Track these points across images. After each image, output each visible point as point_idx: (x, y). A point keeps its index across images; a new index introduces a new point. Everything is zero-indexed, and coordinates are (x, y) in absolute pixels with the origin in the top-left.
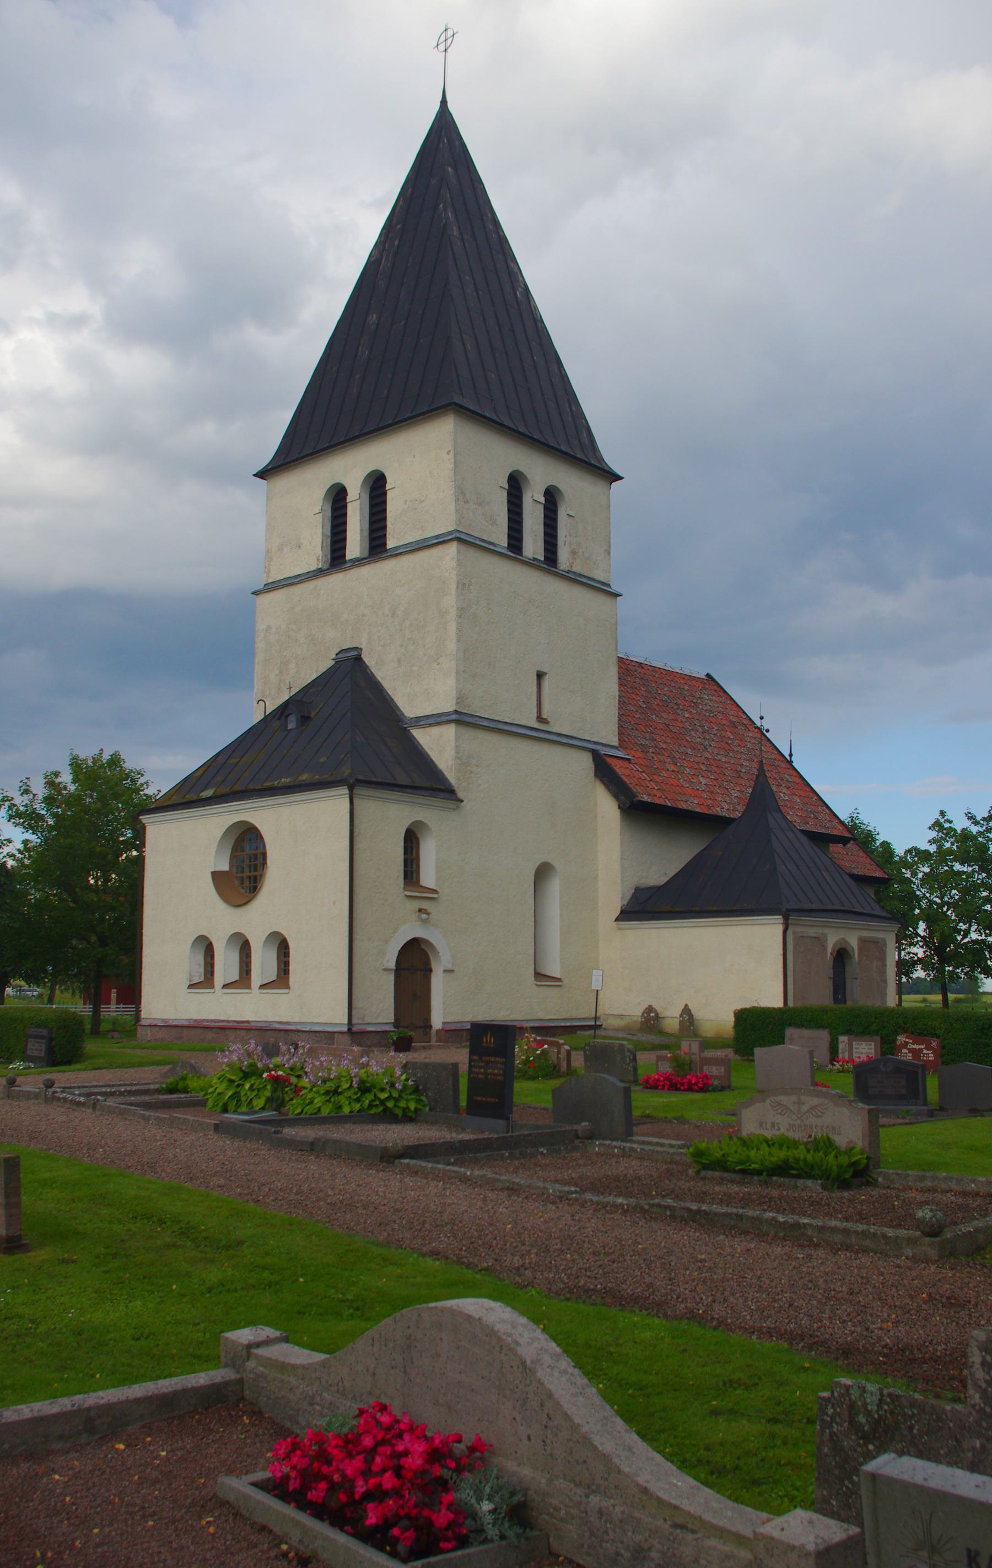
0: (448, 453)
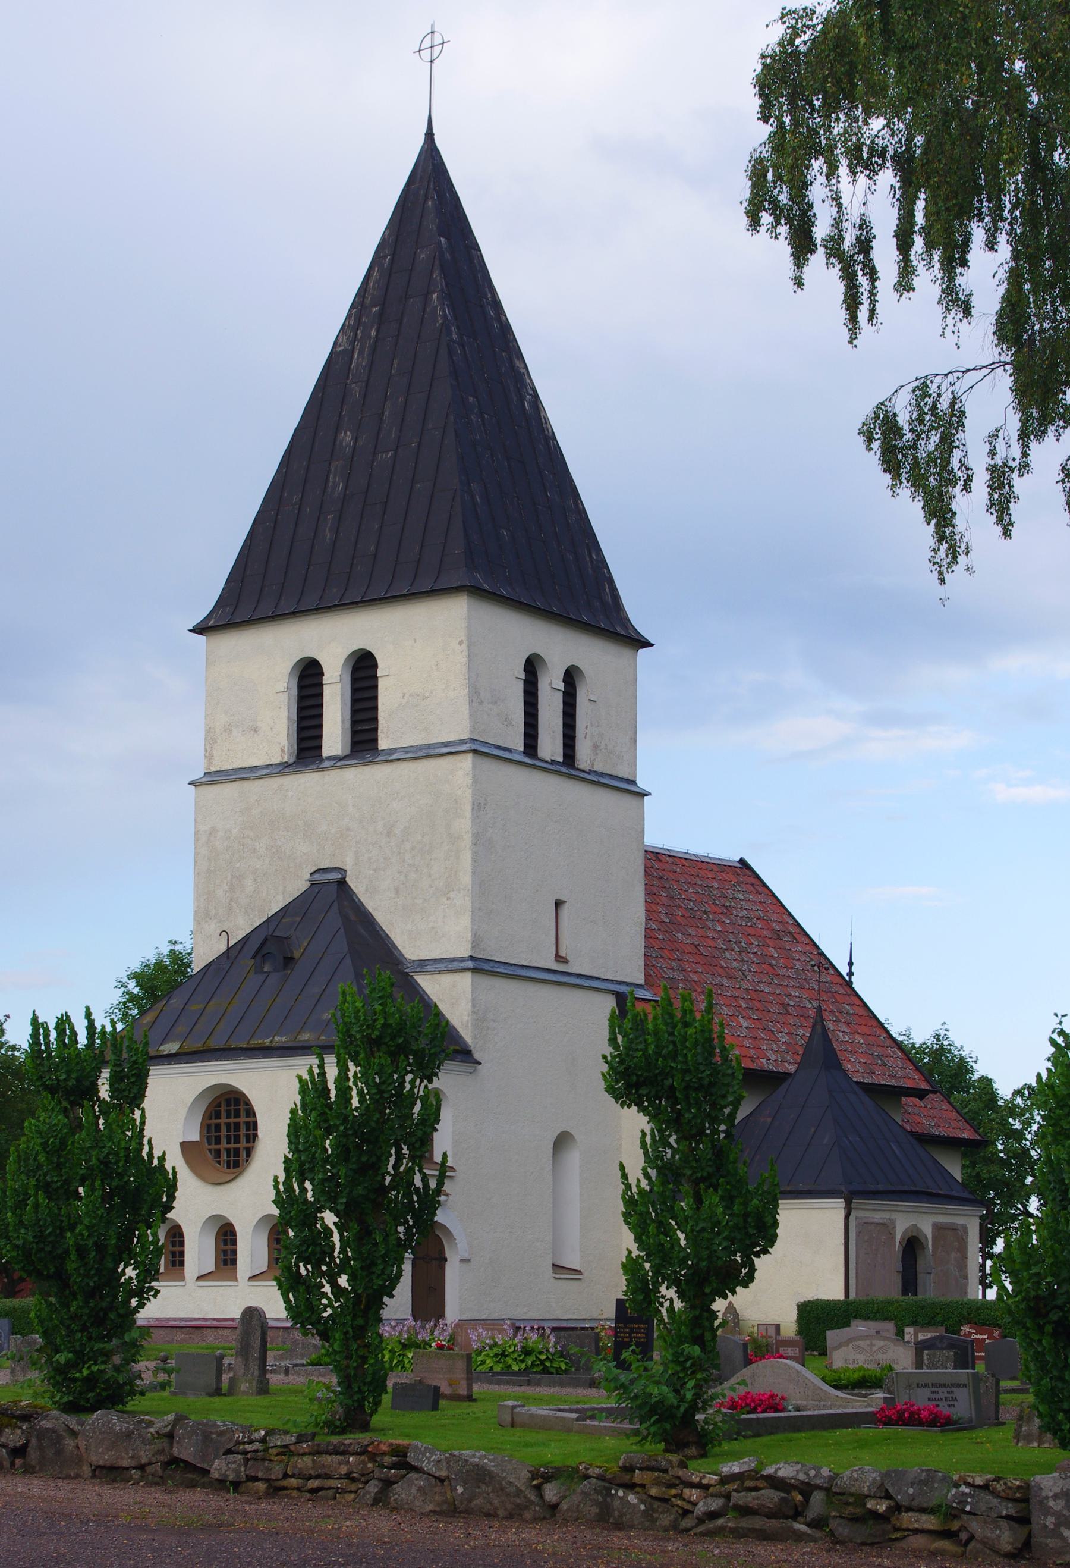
0: (461, 643)
